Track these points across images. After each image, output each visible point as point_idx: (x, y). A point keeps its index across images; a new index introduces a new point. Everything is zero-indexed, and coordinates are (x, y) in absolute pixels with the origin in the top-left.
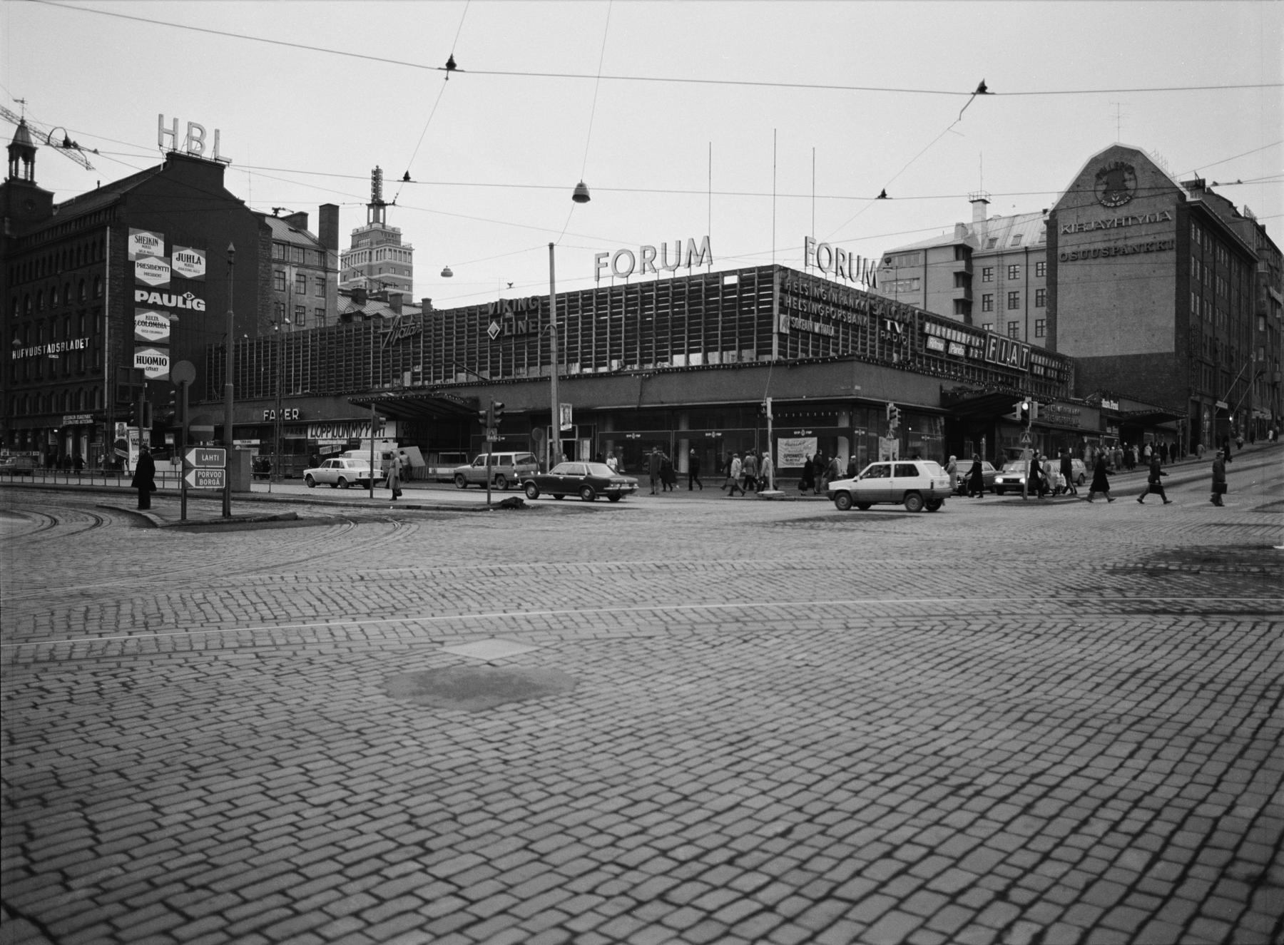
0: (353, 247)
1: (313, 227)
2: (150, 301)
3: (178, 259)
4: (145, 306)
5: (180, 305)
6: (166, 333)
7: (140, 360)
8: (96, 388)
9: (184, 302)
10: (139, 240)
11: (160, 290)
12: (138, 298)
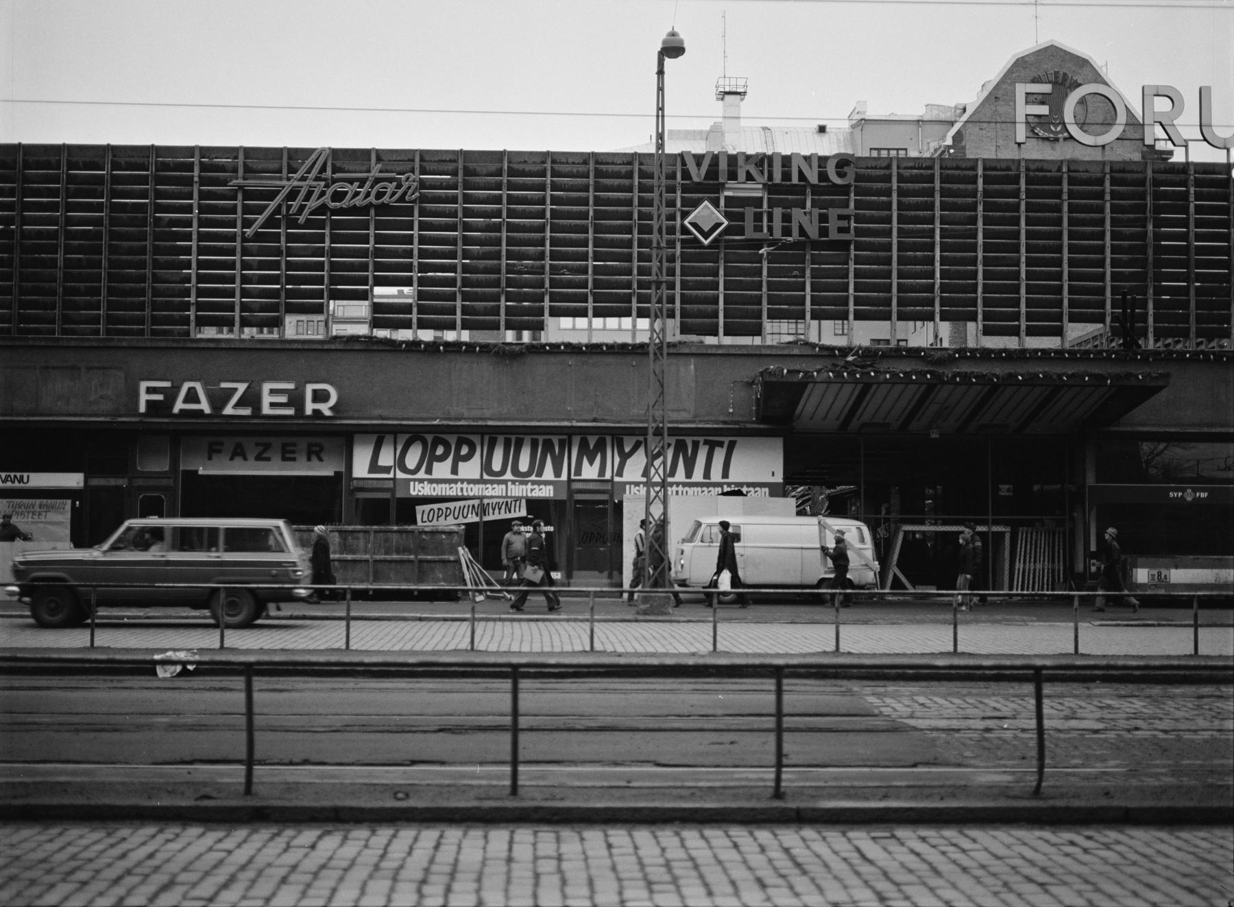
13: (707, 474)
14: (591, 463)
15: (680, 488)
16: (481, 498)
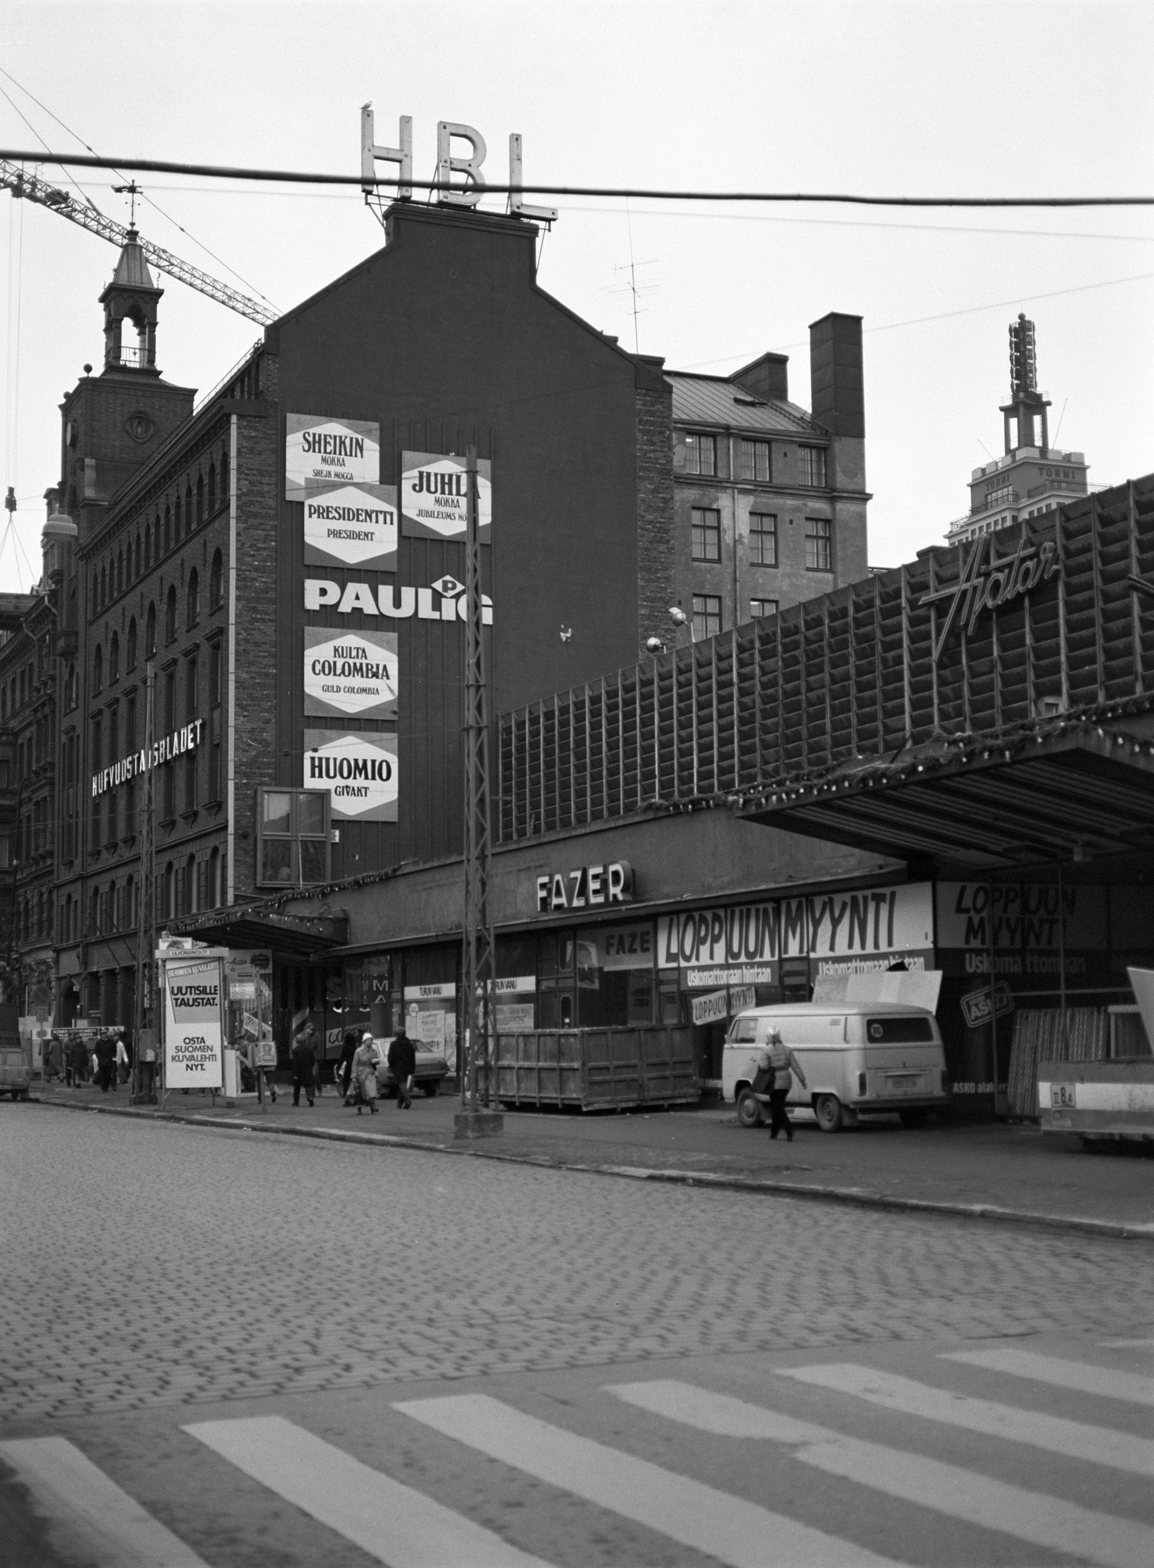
0: (975, 511)
2: (345, 608)
3: (416, 488)
4: (330, 617)
6: (386, 691)
7: (319, 768)
8: (215, 850)
9: (437, 606)
10: (314, 444)
12: (312, 601)
13: (876, 946)
14: (975, 938)
15: (858, 964)
16: (728, 987)
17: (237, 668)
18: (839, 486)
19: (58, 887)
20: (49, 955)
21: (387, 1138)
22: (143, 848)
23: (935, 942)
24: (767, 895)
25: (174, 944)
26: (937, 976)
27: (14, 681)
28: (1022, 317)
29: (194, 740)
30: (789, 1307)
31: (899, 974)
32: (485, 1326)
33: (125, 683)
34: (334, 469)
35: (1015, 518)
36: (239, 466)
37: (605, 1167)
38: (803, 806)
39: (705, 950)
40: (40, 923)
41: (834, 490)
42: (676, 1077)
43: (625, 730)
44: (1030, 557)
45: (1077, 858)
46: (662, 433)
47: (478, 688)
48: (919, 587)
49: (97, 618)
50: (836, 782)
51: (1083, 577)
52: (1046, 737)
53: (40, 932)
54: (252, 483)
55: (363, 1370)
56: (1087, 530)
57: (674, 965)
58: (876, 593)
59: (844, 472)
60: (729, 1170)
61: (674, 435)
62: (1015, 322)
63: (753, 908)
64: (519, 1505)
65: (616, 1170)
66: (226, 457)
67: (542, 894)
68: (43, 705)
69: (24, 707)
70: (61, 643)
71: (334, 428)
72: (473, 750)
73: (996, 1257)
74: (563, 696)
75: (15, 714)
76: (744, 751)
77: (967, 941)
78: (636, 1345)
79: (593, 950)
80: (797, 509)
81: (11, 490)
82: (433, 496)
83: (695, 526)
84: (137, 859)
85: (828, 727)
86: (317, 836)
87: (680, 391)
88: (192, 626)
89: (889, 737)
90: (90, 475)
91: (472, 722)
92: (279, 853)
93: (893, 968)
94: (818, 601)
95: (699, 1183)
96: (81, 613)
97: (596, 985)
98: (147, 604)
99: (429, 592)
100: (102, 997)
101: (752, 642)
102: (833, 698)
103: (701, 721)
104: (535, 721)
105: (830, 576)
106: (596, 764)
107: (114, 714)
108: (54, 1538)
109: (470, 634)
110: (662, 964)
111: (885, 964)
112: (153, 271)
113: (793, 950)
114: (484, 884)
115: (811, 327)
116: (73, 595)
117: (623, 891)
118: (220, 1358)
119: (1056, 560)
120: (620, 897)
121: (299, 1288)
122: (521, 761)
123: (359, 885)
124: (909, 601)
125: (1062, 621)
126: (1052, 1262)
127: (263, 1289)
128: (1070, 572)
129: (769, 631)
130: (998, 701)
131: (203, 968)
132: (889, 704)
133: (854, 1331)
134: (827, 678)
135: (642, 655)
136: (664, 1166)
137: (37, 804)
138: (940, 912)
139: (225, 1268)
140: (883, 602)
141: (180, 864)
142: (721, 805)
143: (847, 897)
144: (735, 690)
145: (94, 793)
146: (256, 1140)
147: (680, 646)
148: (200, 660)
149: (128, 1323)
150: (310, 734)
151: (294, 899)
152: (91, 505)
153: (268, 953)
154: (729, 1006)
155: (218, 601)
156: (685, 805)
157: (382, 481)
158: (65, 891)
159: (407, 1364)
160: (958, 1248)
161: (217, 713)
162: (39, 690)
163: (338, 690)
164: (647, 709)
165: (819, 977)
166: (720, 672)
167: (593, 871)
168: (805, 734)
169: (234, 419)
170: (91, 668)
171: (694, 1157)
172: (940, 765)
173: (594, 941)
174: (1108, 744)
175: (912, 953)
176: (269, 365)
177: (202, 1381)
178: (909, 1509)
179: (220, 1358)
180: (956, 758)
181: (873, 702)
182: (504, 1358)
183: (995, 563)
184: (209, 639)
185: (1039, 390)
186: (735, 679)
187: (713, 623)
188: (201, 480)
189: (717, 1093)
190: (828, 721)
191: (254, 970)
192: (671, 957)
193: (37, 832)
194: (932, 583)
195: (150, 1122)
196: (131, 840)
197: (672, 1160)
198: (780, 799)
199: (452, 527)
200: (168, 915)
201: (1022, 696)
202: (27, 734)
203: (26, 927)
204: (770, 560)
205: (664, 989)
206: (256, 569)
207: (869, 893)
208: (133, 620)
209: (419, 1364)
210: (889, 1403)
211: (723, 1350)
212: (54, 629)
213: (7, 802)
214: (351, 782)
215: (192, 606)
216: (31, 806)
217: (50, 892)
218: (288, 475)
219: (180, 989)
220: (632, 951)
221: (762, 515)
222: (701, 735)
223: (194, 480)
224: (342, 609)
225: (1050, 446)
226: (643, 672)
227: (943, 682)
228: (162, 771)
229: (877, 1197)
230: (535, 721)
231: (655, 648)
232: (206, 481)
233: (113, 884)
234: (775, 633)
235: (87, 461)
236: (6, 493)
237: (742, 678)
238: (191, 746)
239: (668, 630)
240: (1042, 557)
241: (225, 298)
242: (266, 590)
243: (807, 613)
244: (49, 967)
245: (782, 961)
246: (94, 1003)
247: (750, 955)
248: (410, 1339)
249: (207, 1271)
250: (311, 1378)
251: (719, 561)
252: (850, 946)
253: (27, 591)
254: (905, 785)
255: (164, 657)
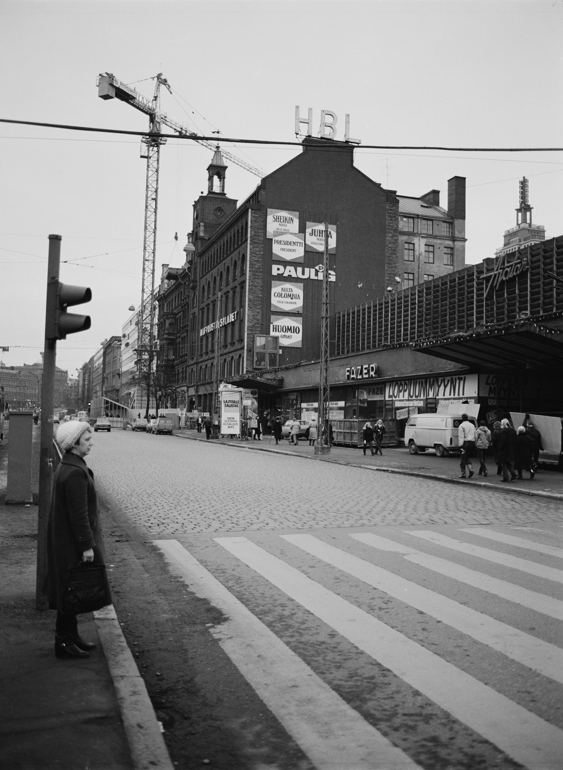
0: (505, 245)
1: (444, 203)
2: (286, 275)
3: (311, 234)
4: (281, 278)
5: (313, 277)
6: (299, 303)
7: (276, 329)
8: (240, 355)
9: (317, 275)
10: (277, 219)
11: (294, 264)
12: (275, 272)
13: (459, 395)
15: (452, 401)
16: (409, 407)
17: (249, 294)
18: (456, 236)
19: (189, 366)
20: (185, 388)
21: (292, 453)
22: (216, 354)
23: (478, 394)
24: (422, 377)
25: (225, 386)
26: (478, 406)
27: (175, 297)
28: (524, 178)
29: (234, 318)
30: (414, 512)
31: (466, 405)
32: (313, 514)
33: (212, 299)
34: (283, 228)
35: (519, 248)
36: (251, 226)
37: (362, 466)
38: (435, 347)
39: (401, 394)
40: (183, 377)
41: (454, 237)
42: (390, 437)
43: (379, 319)
44: (519, 263)
45: (527, 368)
46: (395, 217)
47: (327, 304)
48: (480, 272)
49: (203, 276)
50: (446, 339)
51: (537, 271)
52: (516, 326)
53: (182, 381)
54: (255, 232)
55: (272, 524)
56: (539, 254)
57: (391, 399)
58: (466, 274)
59: (458, 231)
60: (403, 468)
61: (399, 218)
62: (522, 179)
63: (418, 381)
64: (314, 567)
65: (366, 466)
66: (247, 223)
67: (348, 374)
68: (185, 305)
69: (178, 306)
70: (191, 285)
71: (284, 214)
72: (324, 325)
73: (485, 499)
74: (358, 307)
75: (176, 308)
76: (419, 327)
77: (489, 395)
78: (361, 522)
79: (365, 393)
80: (441, 244)
81: (176, 233)
82: (316, 237)
83: (406, 249)
84: (214, 358)
85: (448, 319)
86: (274, 351)
87: (402, 202)
88: (234, 280)
89: (468, 324)
90: (202, 228)
91: (324, 315)
92: (261, 357)
93: (464, 403)
94: (446, 276)
95: (393, 472)
96: (198, 275)
97: (366, 405)
98: (220, 272)
99: (314, 270)
100: (202, 403)
101: (423, 290)
102: (450, 310)
103: (405, 316)
104: (348, 315)
105: (452, 267)
106: (369, 330)
107: (208, 309)
108: (170, 568)
109: (324, 285)
110: (387, 398)
111: (461, 401)
112: (224, 159)
113: (431, 396)
114: (327, 370)
115: (448, 181)
116: (196, 269)
117: (375, 373)
118: (228, 519)
119: (527, 264)
120: (374, 376)
121: (255, 499)
122: (343, 328)
123: (287, 369)
124: (476, 277)
125: (529, 285)
126: (503, 502)
127: (244, 499)
128: (532, 268)
129: (429, 286)
130: (506, 312)
131: (234, 394)
132: (469, 312)
133: (432, 520)
134: (448, 302)
135: (386, 293)
136: (382, 466)
137: (182, 338)
138: (480, 384)
139: (233, 492)
140: (468, 277)
141: (229, 359)
142: (408, 345)
143: (449, 378)
144: (417, 306)
145: (201, 335)
146: (249, 452)
147: (399, 290)
148: (237, 291)
149: (200, 507)
150: (273, 317)
151: (266, 373)
152: (202, 239)
153: (257, 390)
154: (409, 414)
155: (243, 271)
156: (396, 345)
157: (299, 232)
158: (191, 367)
159: (286, 523)
160: (474, 496)
161: (242, 309)
162: (183, 300)
163: (283, 302)
164: (387, 312)
165: (439, 405)
166: (412, 300)
167: (365, 366)
168: (440, 322)
169: (250, 210)
170: (201, 293)
171: (392, 463)
172: (481, 335)
173: (365, 390)
174: (538, 329)
175: (470, 398)
176: (262, 192)
177: (221, 526)
178: (436, 575)
179: (228, 519)
180: (486, 332)
181: (463, 311)
182: (317, 524)
183: (506, 265)
184: (240, 284)
185: (529, 204)
186: (417, 302)
187: (411, 283)
188: (238, 231)
189: (403, 442)
190: (448, 317)
191: (251, 396)
192: (390, 396)
193: (182, 347)
194: (485, 271)
195: (216, 444)
196: (213, 351)
197: (385, 464)
198: (427, 344)
199: (321, 248)
200: (224, 376)
201: (514, 311)
202: (180, 315)
203: (178, 379)
204: (431, 261)
205: (387, 407)
206: (256, 261)
207: (457, 377)
208: (215, 277)
209: (290, 524)
210: (438, 543)
211: (389, 524)
212: (189, 280)
213: (172, 337)
214: (286, 334)
215: (227, 279)
216: (180, 339)
217: (186, 368)
218: (268, 229)
219: (226, 401)
220: (377, 394)
221: (429, 245)
222: (404, 321)
223: (236, 231)
224: (284, 275)
225: (532, 223)
226: (386, 299)
227: (487, 305)
228: (223, 329)
229: (450, 479)
230: (348, 315)
231: (390, 291)
232: (240, 231)
233: (206, 365)
234: (431, 287)
235: (201, 224)
236: (175, 234)
237: (419, 302)
238: (233, 320)
239: (395, 285)
240: (523, 263)
241: (249, 169)
242: (259, 268)
243: (442, 280)
244: (185, 392)
245: (427, 399)
246: (199, 405)
247: (416, 397)
248: (288, 516)
249: (227, 493)
250: (255, 527)
251: (414, 261)
252: (450, 395)
253: (181, 268)
254: (469, 341)
255: (225, 290)
